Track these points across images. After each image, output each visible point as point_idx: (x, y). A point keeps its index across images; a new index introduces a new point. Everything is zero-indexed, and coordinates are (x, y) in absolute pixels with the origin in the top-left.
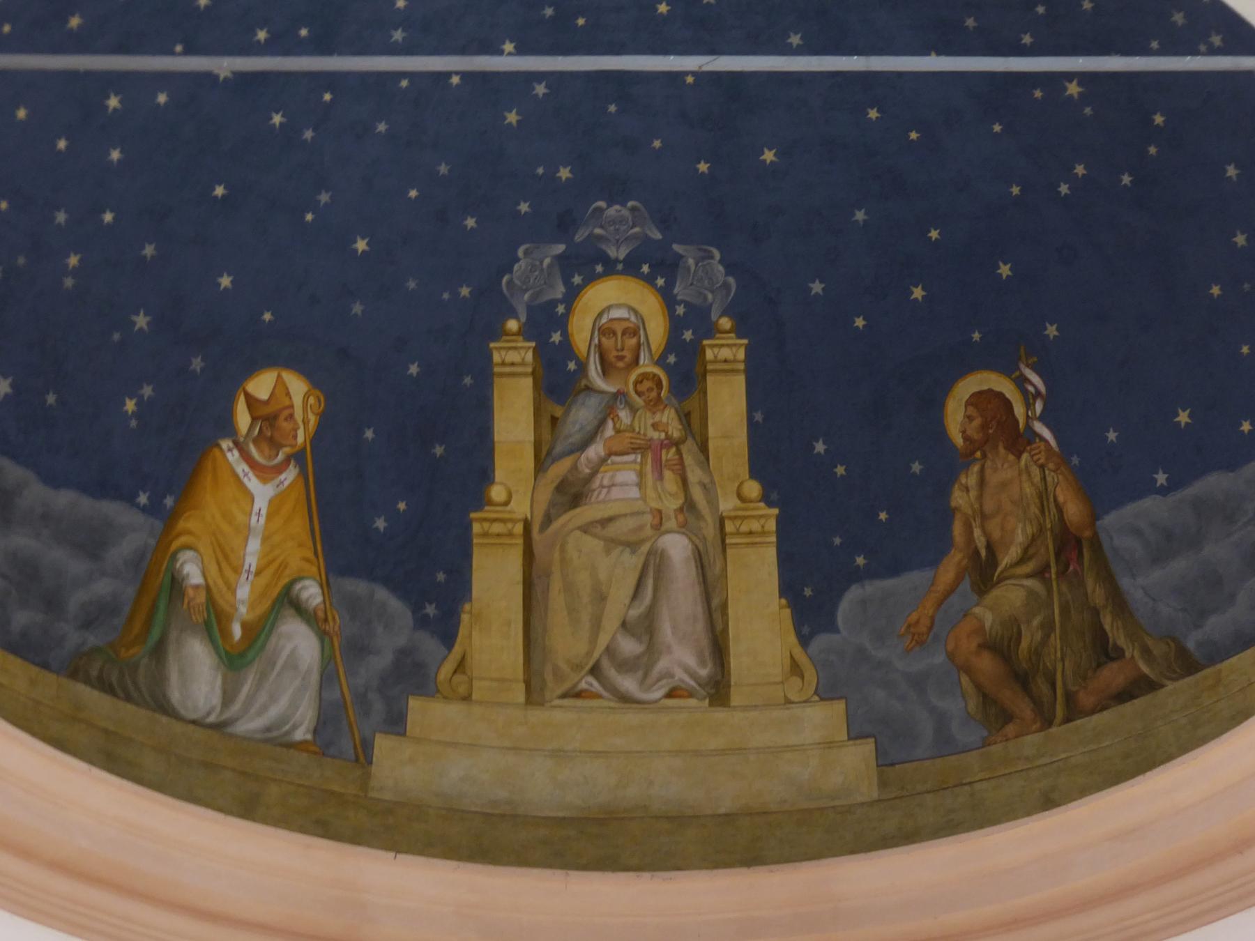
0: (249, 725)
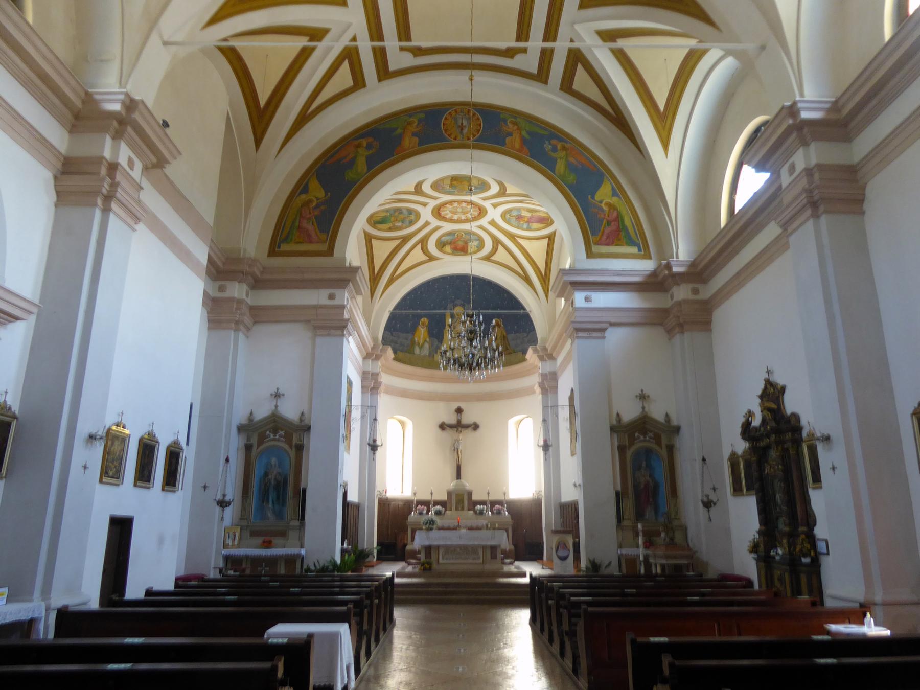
0: (422, 354)
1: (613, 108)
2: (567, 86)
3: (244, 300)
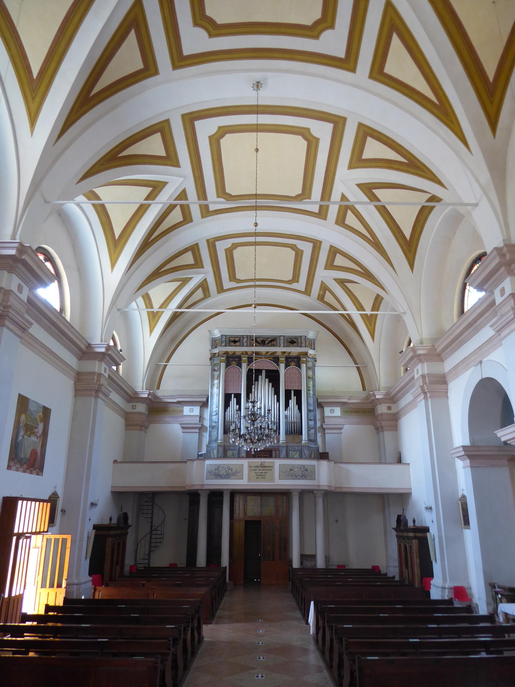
1: (363, 270)
2: (341, 221)
3: (102, 374)
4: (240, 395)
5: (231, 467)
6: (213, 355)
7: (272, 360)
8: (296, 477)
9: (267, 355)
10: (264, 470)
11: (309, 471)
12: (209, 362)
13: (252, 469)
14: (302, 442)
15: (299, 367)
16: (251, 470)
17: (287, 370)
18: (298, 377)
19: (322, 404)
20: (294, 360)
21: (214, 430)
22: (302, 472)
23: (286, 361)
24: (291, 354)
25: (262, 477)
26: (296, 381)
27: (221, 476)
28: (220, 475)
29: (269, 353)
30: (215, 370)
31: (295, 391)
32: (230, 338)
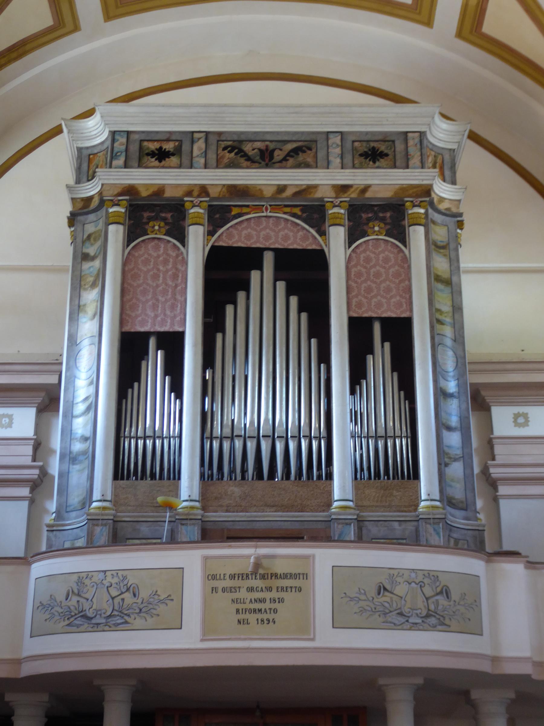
4: (180, 337)
5: (131, 581)
6: (80, 205)
7: (294, 215)
8: (402, 620)
9: (280, 196)
10: (269, 589)
11: (455, 596)
12: (67, 231)
13: (220, 584)
14: (417, 505)
15: (403, 238)
16: (214, 590)
17: (353, 251)
18: (397, 275)
19: (483, 393)
20: (381, 215)
21: (77, 467)
22: (427, 599)
23: (349, 220)
24: (368, 195)
25: (260, 616)
26: (388, 290)
27: (91, 619)
28: (85, 617)
29: (289, 192)
30: (86, 257)
31: (386, 322)
32: (145, 144)
